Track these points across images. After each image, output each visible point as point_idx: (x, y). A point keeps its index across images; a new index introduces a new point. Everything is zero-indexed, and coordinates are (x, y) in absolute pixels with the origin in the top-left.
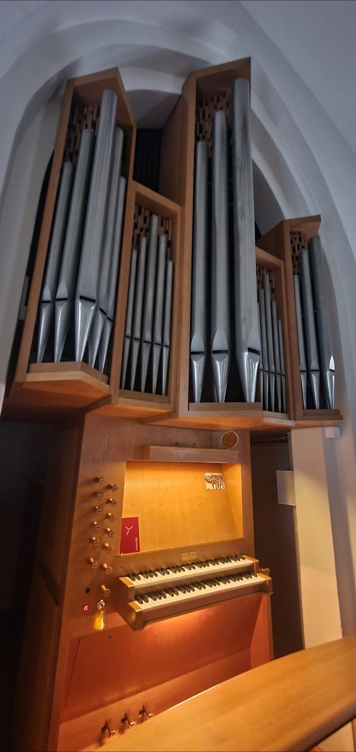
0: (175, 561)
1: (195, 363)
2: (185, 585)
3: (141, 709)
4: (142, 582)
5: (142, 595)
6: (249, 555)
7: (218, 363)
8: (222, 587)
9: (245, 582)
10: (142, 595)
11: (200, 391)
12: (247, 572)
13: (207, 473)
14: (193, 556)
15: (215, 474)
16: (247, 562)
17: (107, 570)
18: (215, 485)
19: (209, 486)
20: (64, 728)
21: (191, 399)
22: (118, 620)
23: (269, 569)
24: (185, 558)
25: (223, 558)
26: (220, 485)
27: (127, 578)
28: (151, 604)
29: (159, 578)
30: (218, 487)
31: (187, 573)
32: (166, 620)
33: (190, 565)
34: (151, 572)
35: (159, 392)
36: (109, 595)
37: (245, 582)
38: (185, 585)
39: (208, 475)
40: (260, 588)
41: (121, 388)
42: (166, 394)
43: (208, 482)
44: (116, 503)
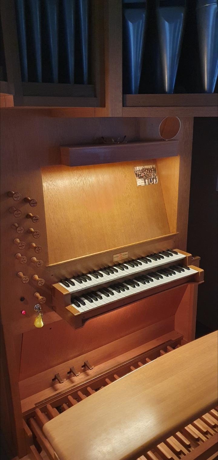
0: (106, 261)
1: (130, 25)
2: (118, 285)
3: (83, 364)
4: (77, 286)
5: (77, 298)
6: (182, 249)
7: (167, 24)
8: (155, 283)
9: (178, 275)
10: (77, 298)
11: (139, 74)
12: (180, 265)
13: (137, 167)
14: (125, 255)
15: (147, 167)
16: (180, 256)
17: (39, 282)
18: (146, 181)
19: (140, 182)
20: (21, 383)
21: (126, 89)
22: (55, 317)
23: (200, 257)
24: (117, 258)
25: (155, 254)
26: (153, 179)
27: (61, 284)
28: (88, 306)
29: (94, 282)
30: (151, 182)
31: (120, 274)
32: (100, 317)
33: (121, 265)
34: (83, 275)
35: (79, 80)
36: (44, 302)
37: (178, 275)
38: (118, 285)
39: (139, 168)
40: (191, 279)
41: (23, 80)
42: (91, 81)
43: (139, 178)
44: (38, 219)
